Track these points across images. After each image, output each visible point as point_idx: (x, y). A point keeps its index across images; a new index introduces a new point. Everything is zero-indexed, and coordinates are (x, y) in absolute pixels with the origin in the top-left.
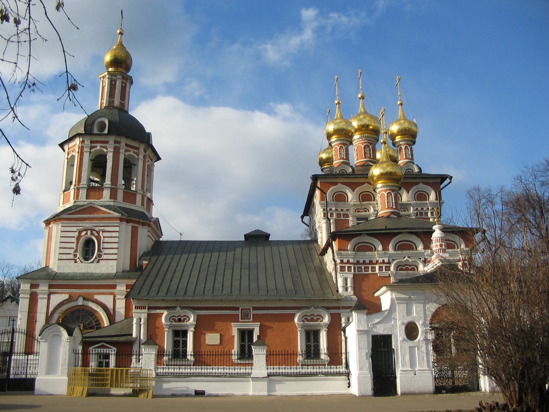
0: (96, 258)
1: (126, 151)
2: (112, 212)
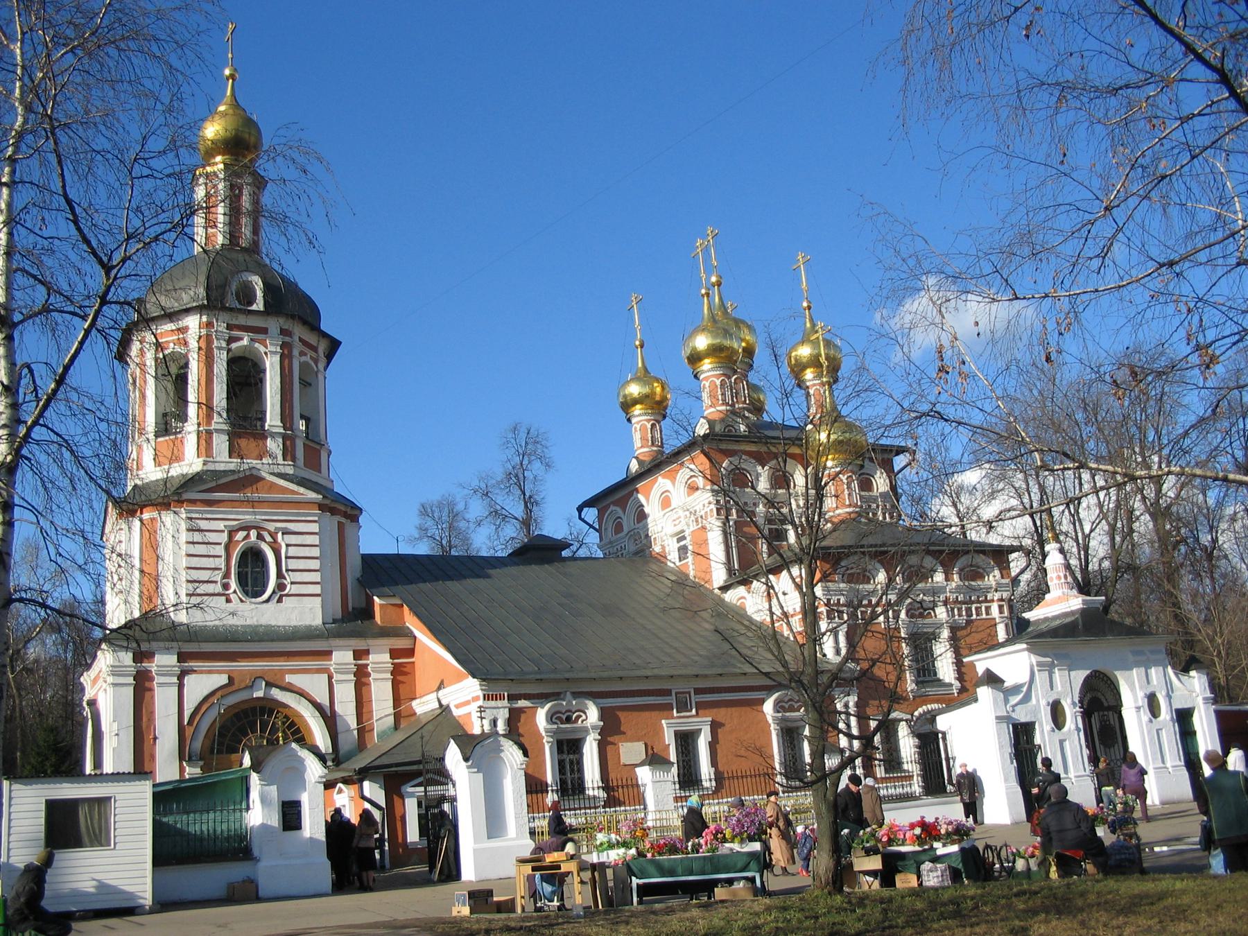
0: (274, 592)
1: (302, 354)
2: (302, 490)
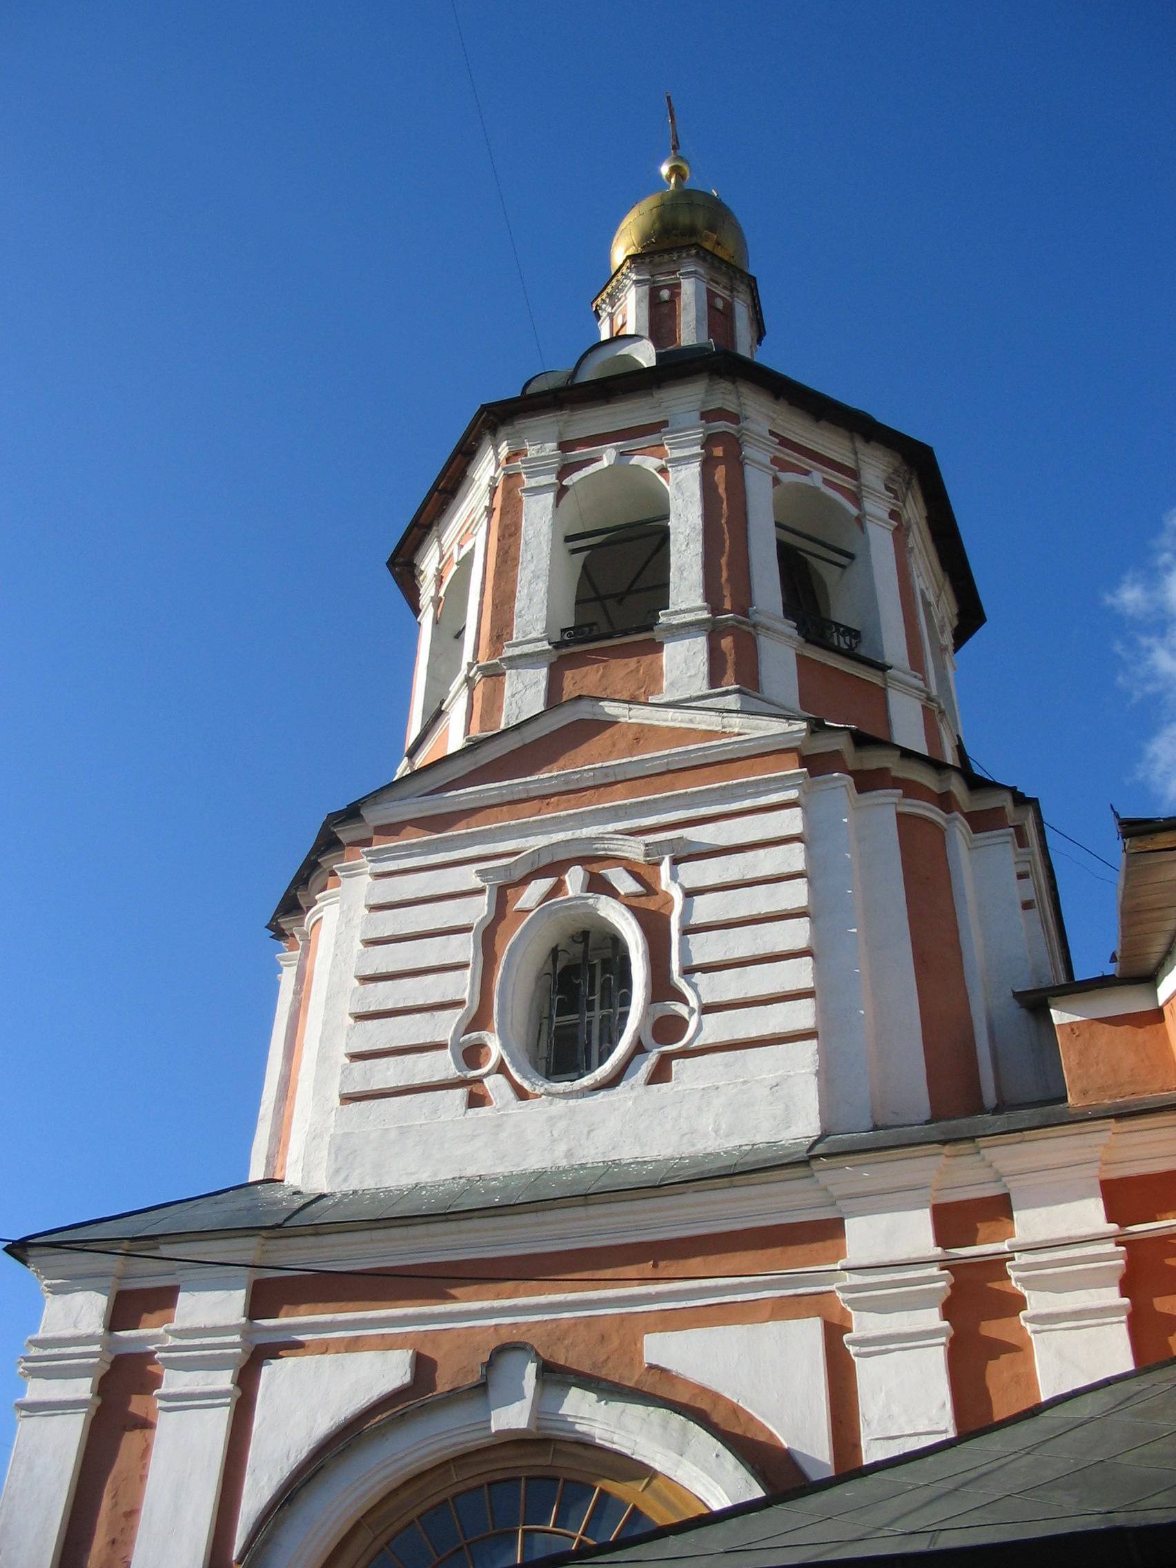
0: (639, 1049)
